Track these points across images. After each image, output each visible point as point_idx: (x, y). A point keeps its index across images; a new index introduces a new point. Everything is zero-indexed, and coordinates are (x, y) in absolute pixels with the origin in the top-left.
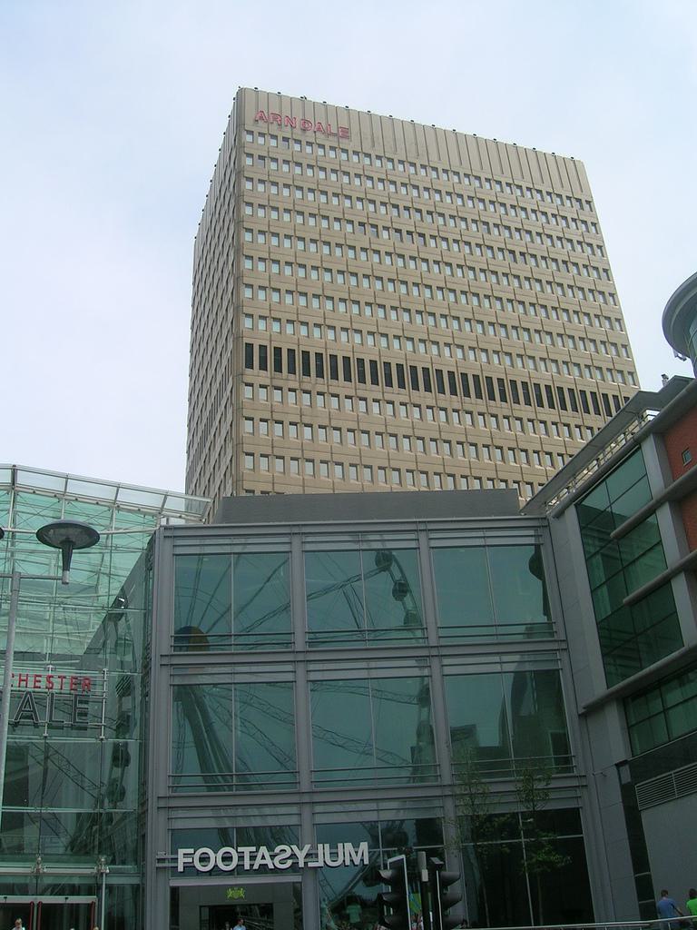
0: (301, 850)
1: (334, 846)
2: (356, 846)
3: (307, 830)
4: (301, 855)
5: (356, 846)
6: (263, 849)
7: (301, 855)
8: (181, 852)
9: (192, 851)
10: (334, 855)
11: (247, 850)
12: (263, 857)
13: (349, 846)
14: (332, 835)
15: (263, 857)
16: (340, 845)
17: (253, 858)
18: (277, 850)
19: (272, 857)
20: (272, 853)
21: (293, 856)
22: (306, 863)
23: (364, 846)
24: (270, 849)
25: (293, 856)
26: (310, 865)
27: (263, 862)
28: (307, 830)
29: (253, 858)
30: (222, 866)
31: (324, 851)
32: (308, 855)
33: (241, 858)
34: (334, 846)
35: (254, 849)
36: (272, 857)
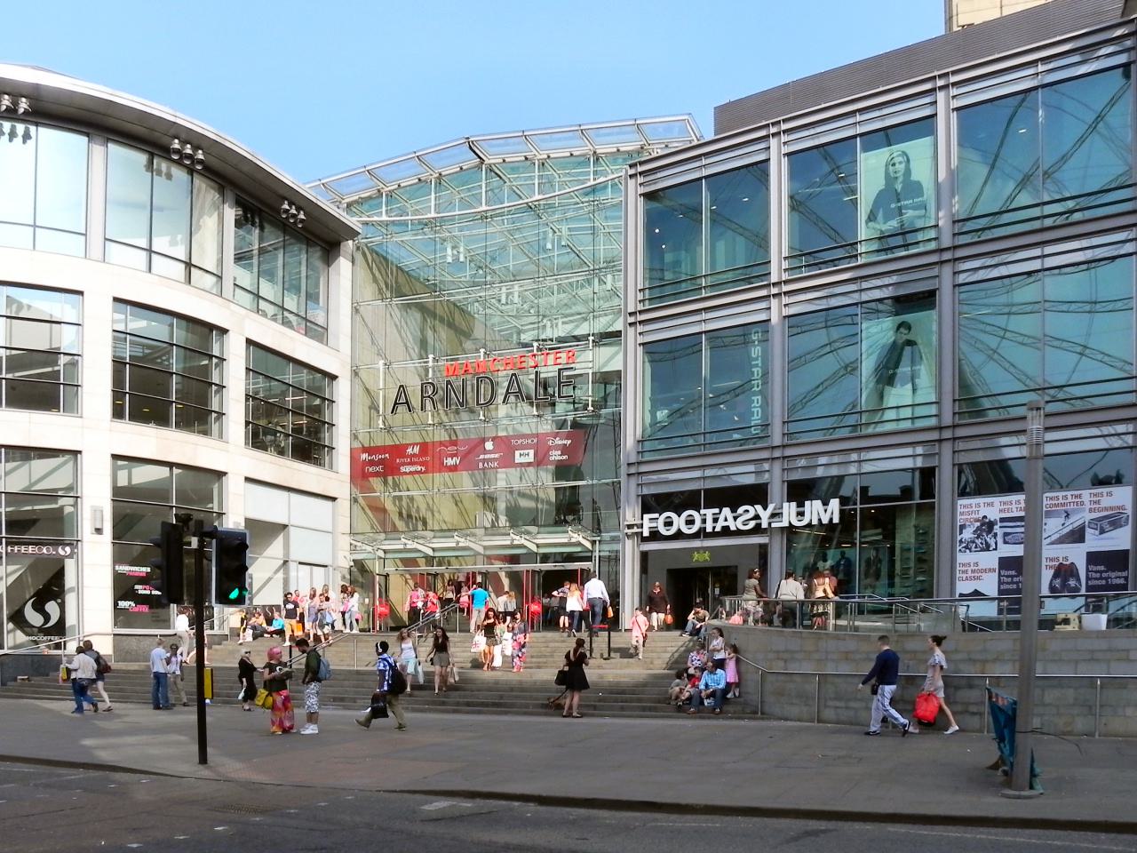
0: (765, 508)
1: (801, 505)
2: (825, 503)
3: (777, 490)
4: (765, 516)
5: (825, 503)
6: (726, 511)
7: (765, 516)
8: (646, 517)
9: (656, 515)
10: (801, 514)
11: (709, 513)
12: (726, 520)
13: (818, 504)
14: (800, 492)
15: (726, 520)
16: (807, 503)
17: (715, 520)
18: (741, 510)
19: (735, 518)
20: (735, 514)
21: (757, 517)
22: (770, 524)
23: (835, 504)
24: (734, 511)
25: (757, 517)
26: (773, 525)
27: (726, 524)
28: (777, 490)
29: (715, 520)
30: (685, 530)
31: (790, 510)
32: (773, 515)
33: (704, 521)
34: (801, 505)
35: (717, 510)
36: (735, 518)
